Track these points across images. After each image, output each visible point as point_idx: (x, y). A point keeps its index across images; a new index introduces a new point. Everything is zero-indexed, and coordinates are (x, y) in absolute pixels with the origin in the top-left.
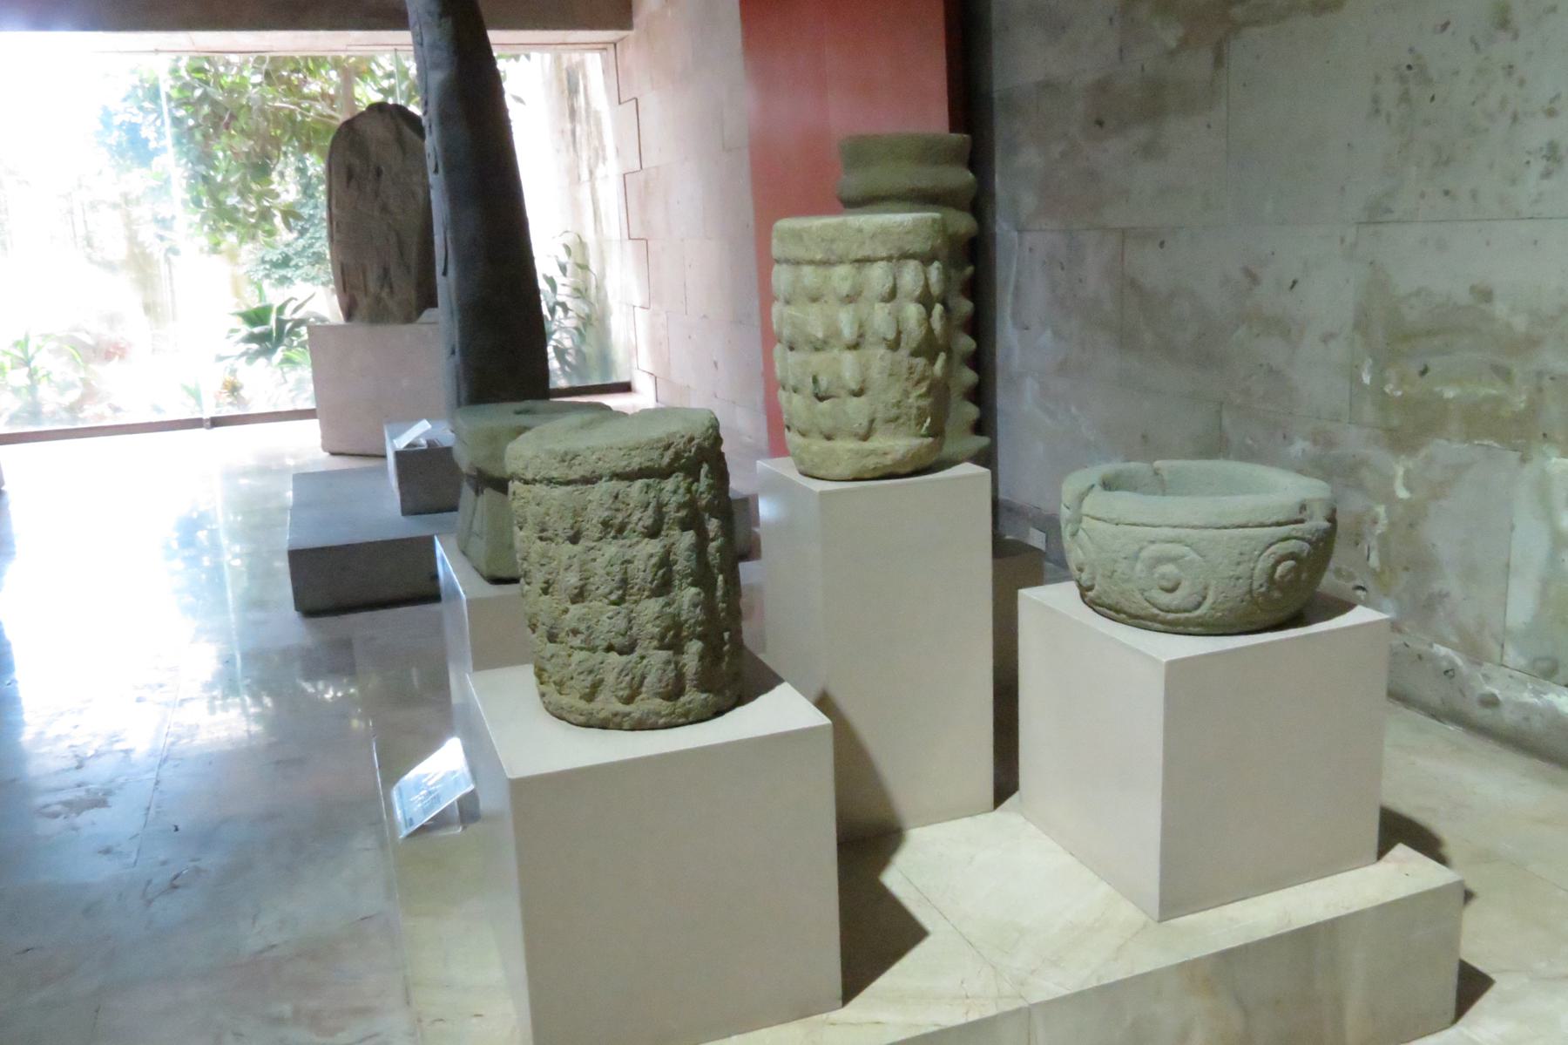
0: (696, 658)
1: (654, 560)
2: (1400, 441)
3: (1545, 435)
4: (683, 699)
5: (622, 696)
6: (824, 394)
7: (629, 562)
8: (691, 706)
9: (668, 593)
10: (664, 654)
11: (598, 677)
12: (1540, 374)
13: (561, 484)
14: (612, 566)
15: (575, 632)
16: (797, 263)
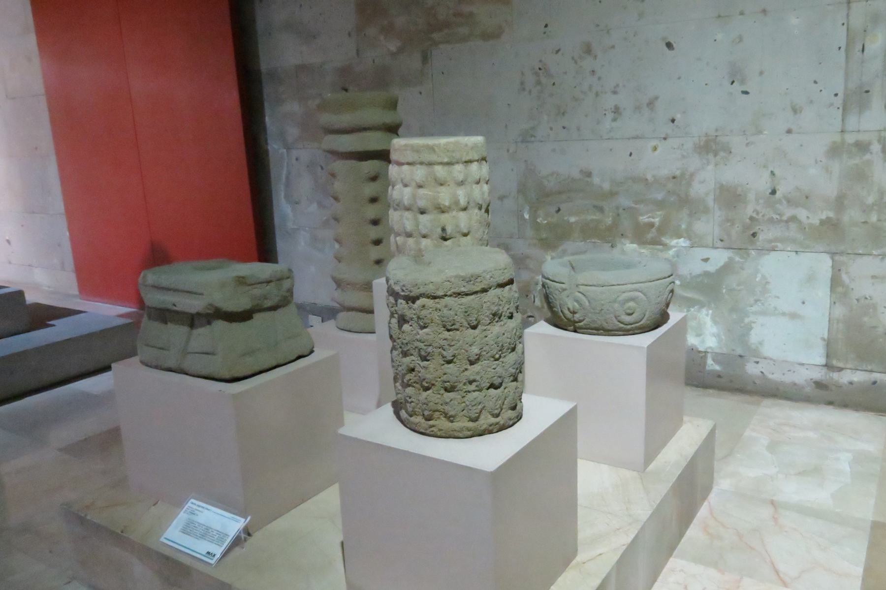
2: (548, 244)
3: (622, 235)
12: (617, 208)
13: (467, 295)
16: (430, 164)
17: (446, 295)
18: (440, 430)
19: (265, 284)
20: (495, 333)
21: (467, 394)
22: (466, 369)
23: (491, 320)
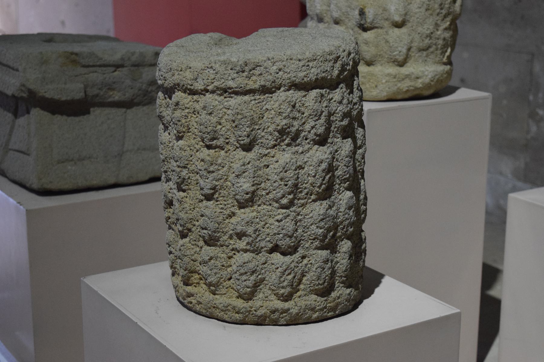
0: (347, 255)
1: (324, 166)
4: (334, 295)
5: (283, 294)
6: (369, 25)
7: (301, 167)
8: (339, 300)
9: (330, 197)
10: (325, 253)
11: (260, 276)
13: (237, 93)
14: (286, 172)
15: (240, 235)
17: (207, 91)
18: (199, 303)
19: (113, 69)
20: (281, 162)
21: (234, 254)
22: (234, 214)
23: (276, 140)
